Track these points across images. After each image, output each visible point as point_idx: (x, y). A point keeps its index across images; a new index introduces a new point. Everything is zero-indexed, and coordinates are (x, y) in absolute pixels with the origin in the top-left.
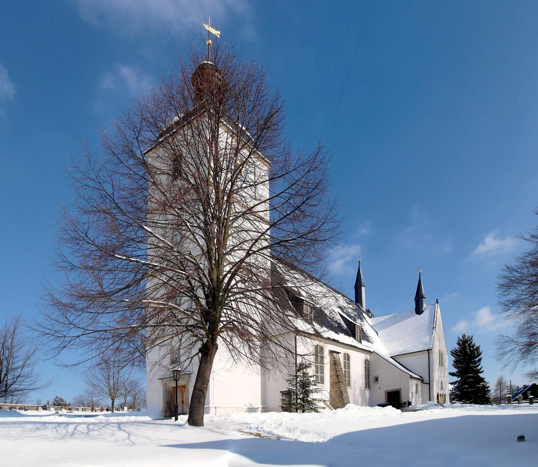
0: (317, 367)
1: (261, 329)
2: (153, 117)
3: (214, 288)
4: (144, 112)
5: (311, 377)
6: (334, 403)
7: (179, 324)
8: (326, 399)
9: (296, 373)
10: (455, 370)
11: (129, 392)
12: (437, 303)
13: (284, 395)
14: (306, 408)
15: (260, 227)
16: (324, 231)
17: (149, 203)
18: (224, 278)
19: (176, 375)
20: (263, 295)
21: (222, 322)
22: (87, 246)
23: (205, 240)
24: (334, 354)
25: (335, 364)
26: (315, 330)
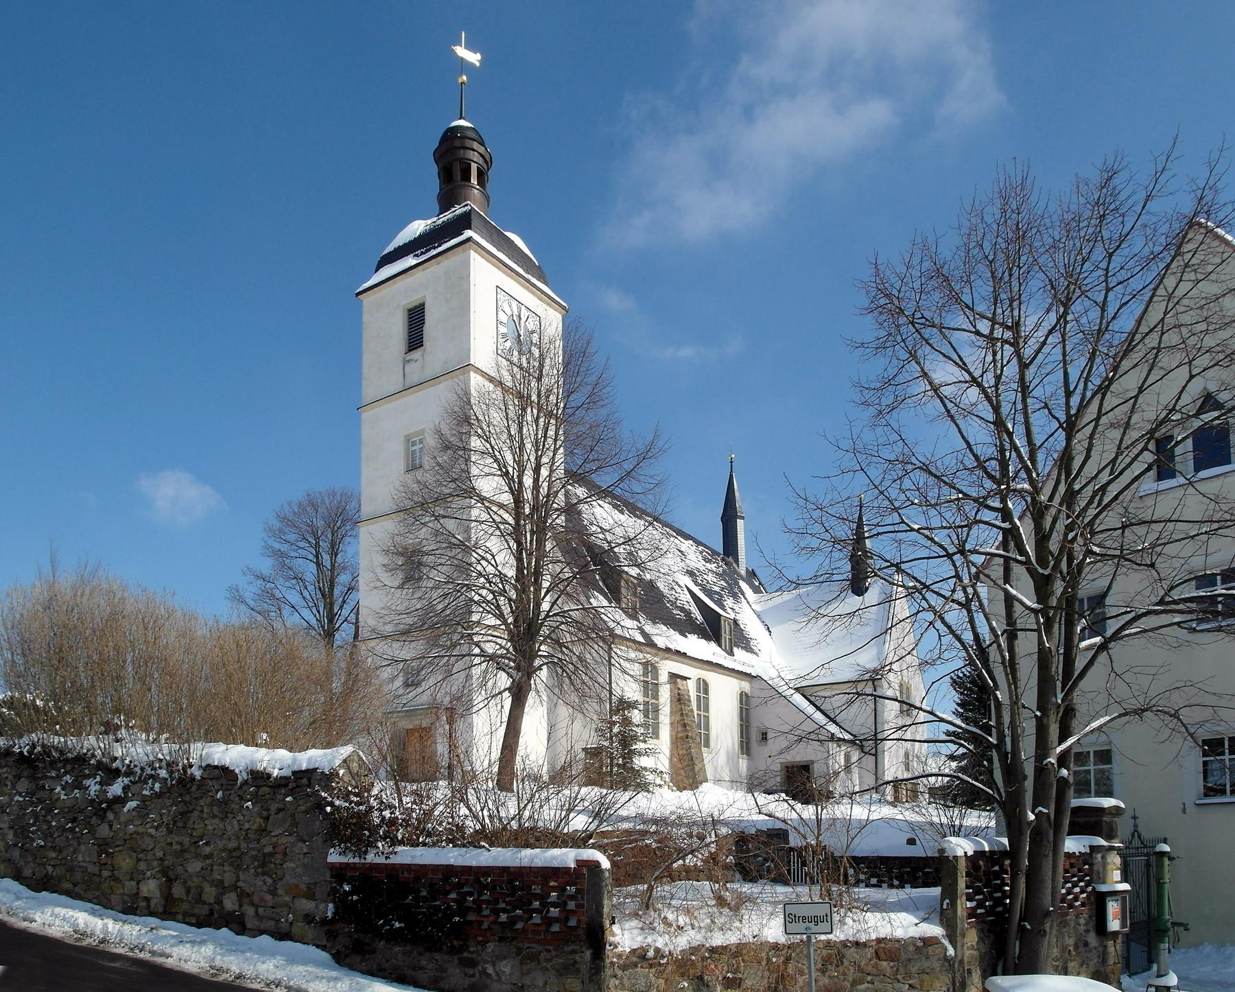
25: (679, 700)
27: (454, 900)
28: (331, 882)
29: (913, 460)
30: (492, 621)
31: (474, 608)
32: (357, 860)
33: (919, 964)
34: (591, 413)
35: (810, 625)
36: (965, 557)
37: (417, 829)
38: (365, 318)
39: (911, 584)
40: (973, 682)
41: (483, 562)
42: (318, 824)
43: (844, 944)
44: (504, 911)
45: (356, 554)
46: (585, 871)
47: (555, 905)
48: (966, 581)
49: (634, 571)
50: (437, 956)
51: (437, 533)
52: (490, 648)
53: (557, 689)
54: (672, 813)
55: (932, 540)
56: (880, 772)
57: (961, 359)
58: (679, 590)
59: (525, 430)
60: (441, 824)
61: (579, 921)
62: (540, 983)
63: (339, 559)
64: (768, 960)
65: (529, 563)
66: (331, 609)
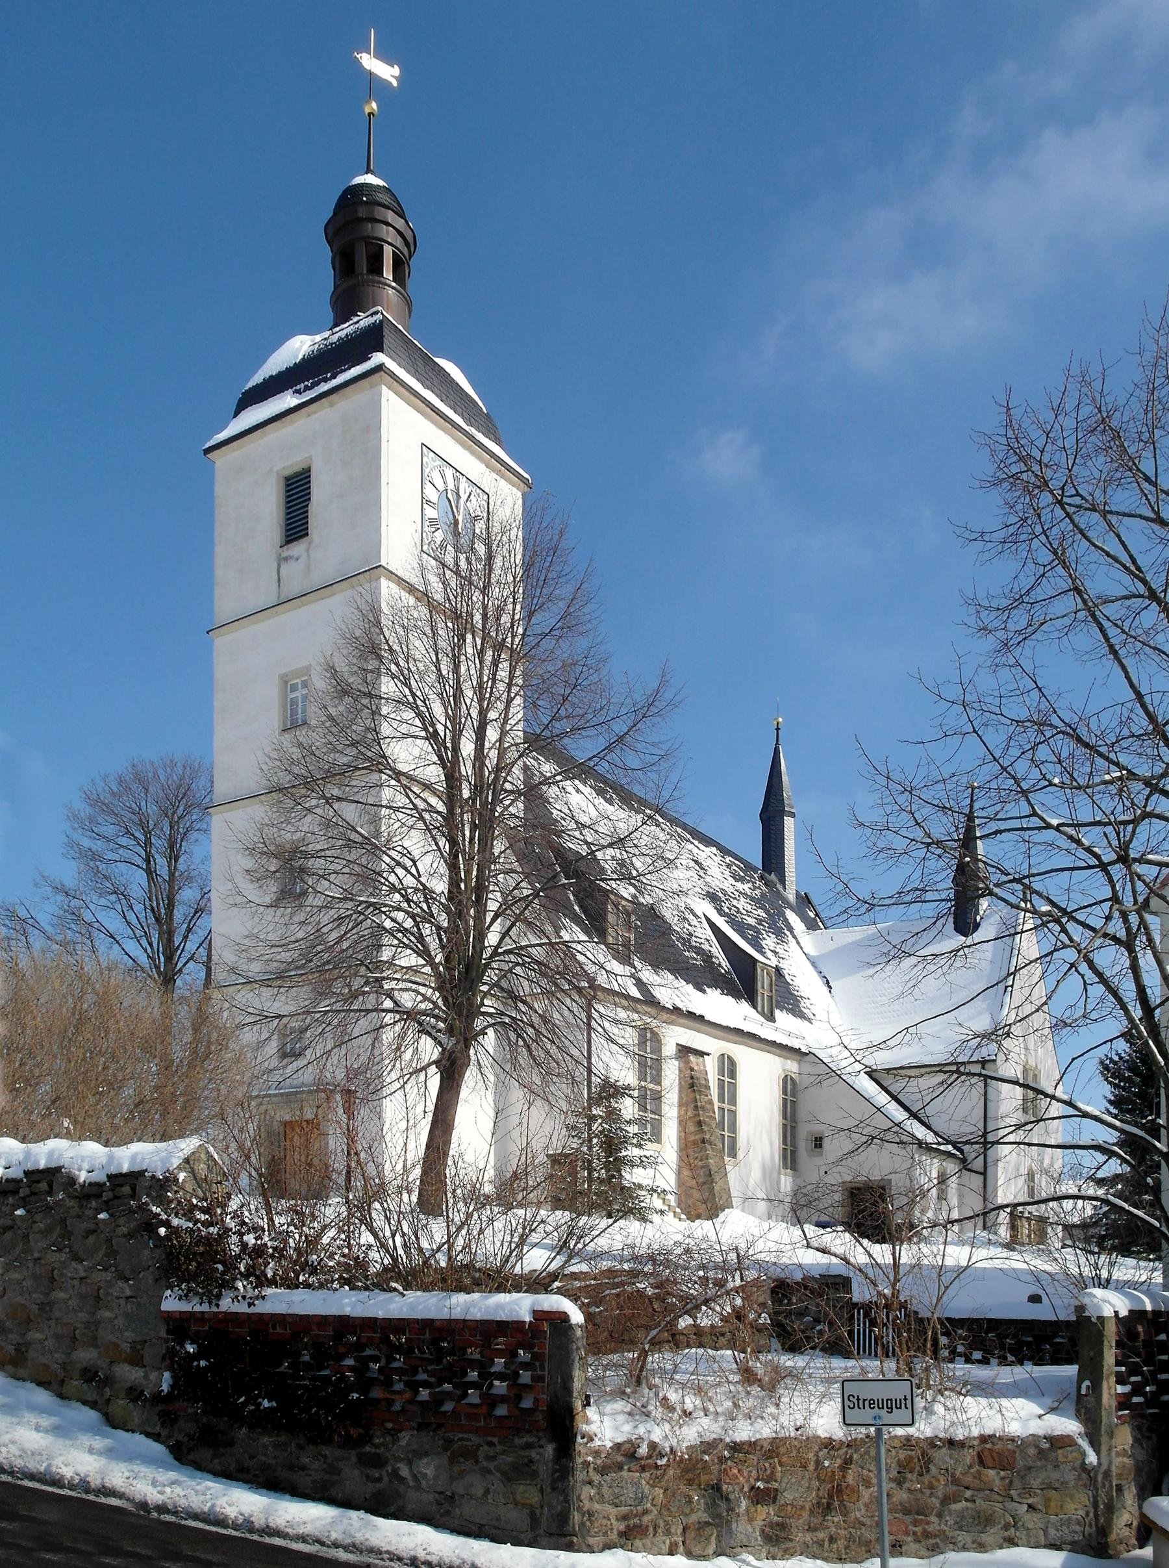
5: (629, 1122)
6: (690, 1202)
8: (668, 1188)
24: (692, 1058)
25: (692, 1086)
27: (351, 1368)
28: (167, 1341)
29: (1055, 720)
30: (409, 959)
31: (386, 939)
32: (205, 1308)
33: (1043, 1475)
34: (564, 644)
35: (889, 967)
36: (1129, 867)
37: (296, 1263)
38: (219, 489)
39: (1045, 908)
40: (1133, 1068)
41: (400, 872)
42: (148, 1254)
43: (932, 1442)
44: (426, 1385)
45: (207, 858)
46: (546, 1326)
47: (501, 1376)
48: (1128, 902)
49: (627, 891)
50: (326, 1451)
51: (328, 824)
52: (407, 1000)
53: (508, 1067)
54: (677, 1244)
55: (1078, 842)
56: (989, 1190)
57: (1134, 561)
58: (694, 922)
59: (463, 669)
60: (331, 1257)
61: (536, 1400)
62: (479, 1491)
63: (182, 865)
64: (818, 1463)
65: (468, 872)
66: (170, 940)
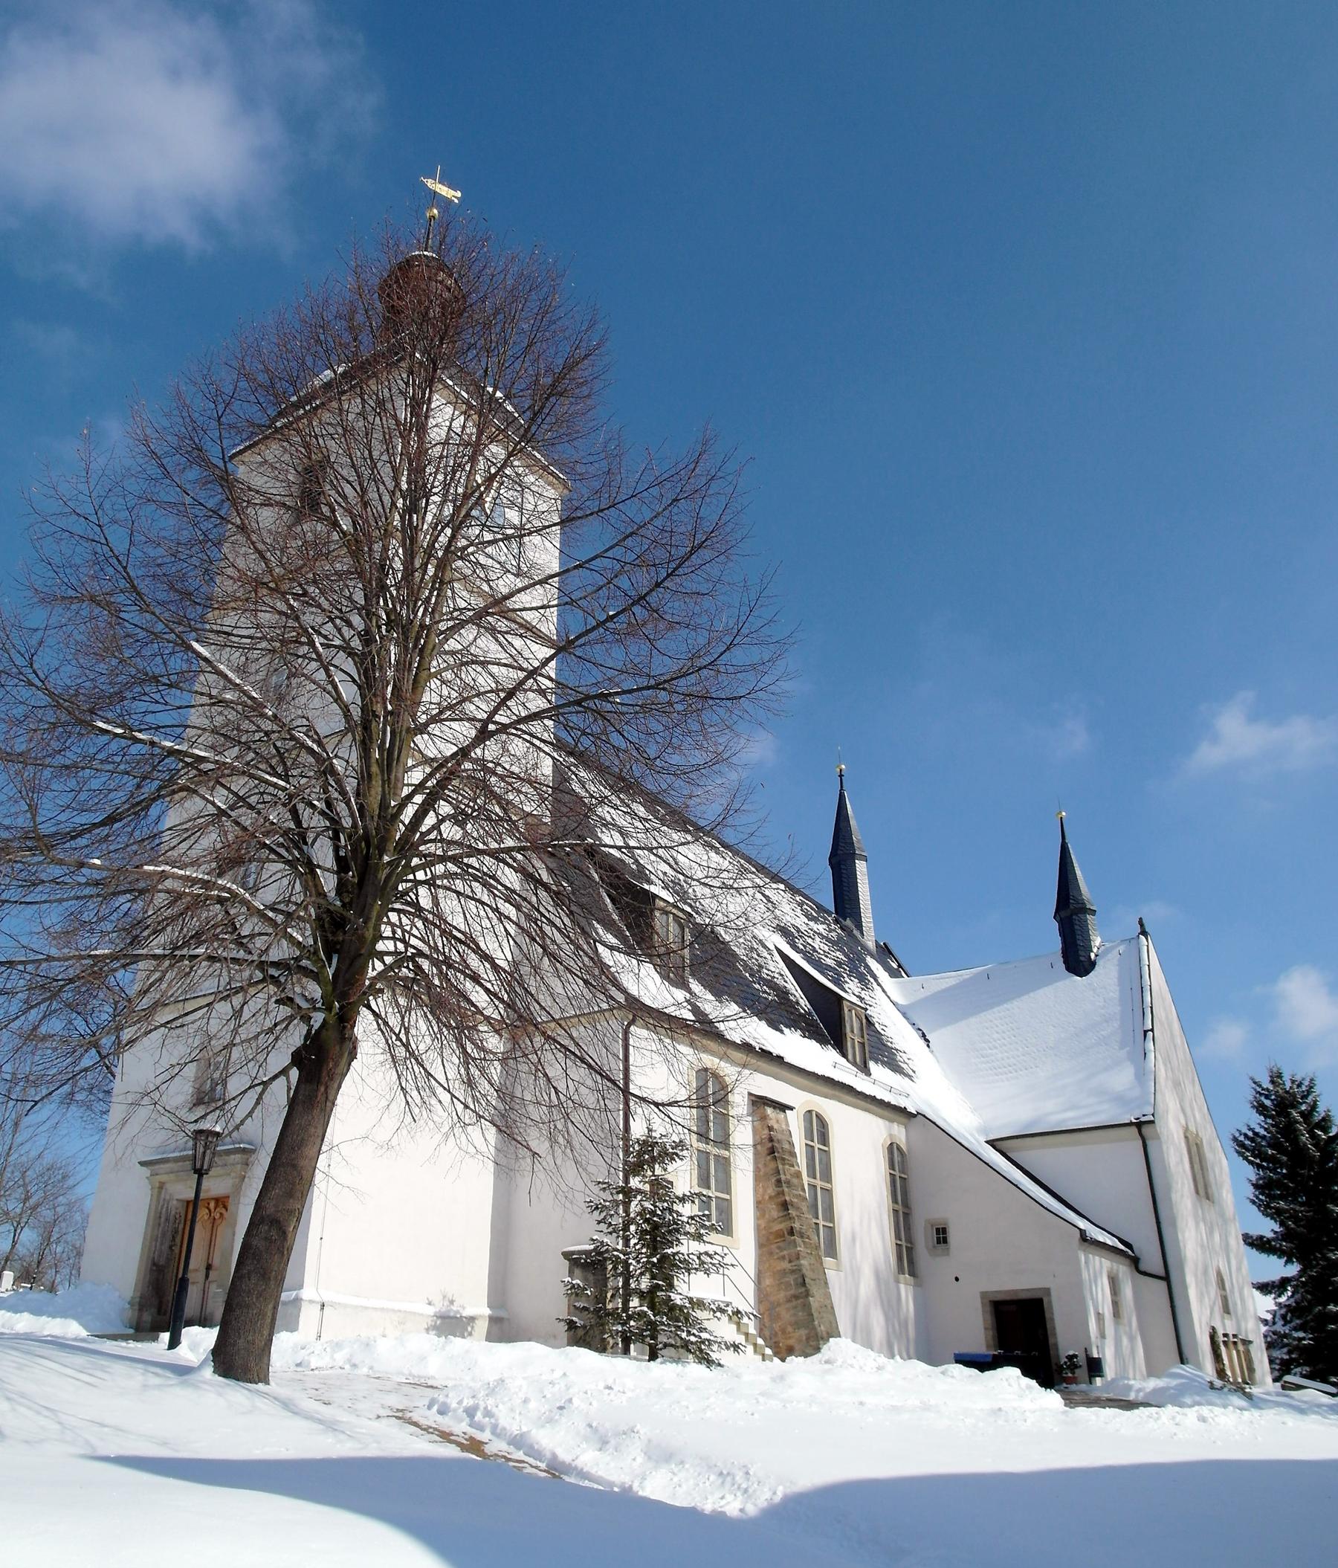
0: (704, 1157)
1: (511, 991)
2: (267, 370)
3: (366, 837)
4: (248, 359)
5: (682, 1200)
6: (776, 1327)
7: (242, 954)
8: (744, 1307)
9: (626, 1181)
10: (1267, 1227)
11: (34, 1208)
12: (1144, 933)
13: (577, 1271)
14: (662, 1338)
15: (527, 654)
16: (731, 669)
17: (218, 579)
18: (402, 806)
19: (203, 1152)
20: (521, 870)
21: (380, 956)
22: (25, 693)
23: (360, 687)
24: (769, 1111)
25: (772, 1151)
26: (696, 1010)
